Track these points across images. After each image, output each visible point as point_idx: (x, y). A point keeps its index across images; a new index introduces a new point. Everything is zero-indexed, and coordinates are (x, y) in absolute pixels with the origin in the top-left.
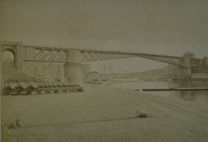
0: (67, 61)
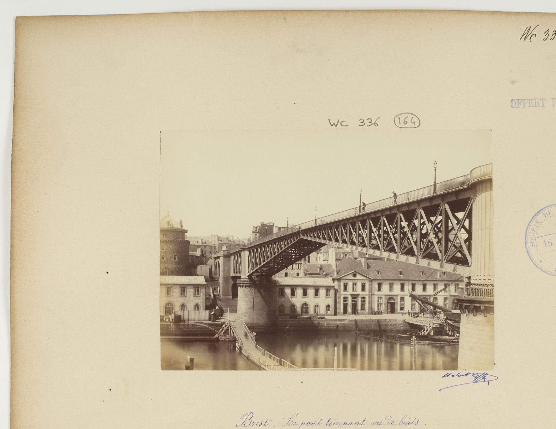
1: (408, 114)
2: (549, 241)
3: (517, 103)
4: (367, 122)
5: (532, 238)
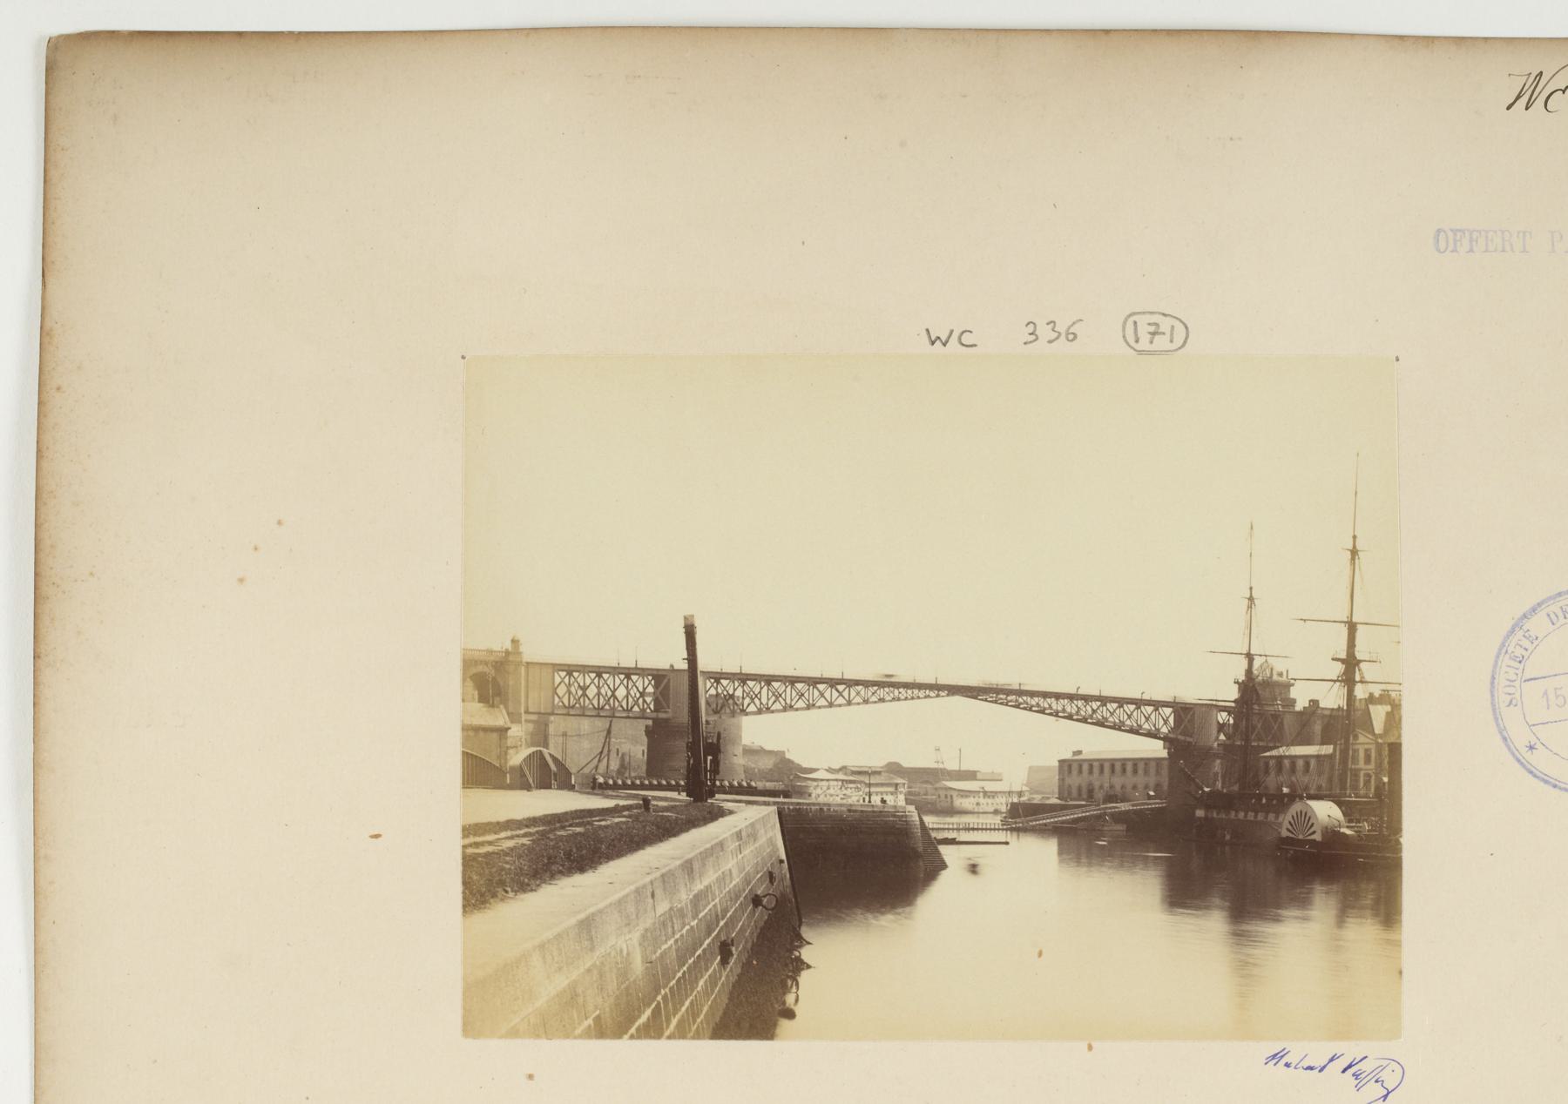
0: (662, 715)
1: (1178, 322)
2: (1559, 693)
3: (1451, 241)
4: (1045, 332)
5: (1513, 681)
